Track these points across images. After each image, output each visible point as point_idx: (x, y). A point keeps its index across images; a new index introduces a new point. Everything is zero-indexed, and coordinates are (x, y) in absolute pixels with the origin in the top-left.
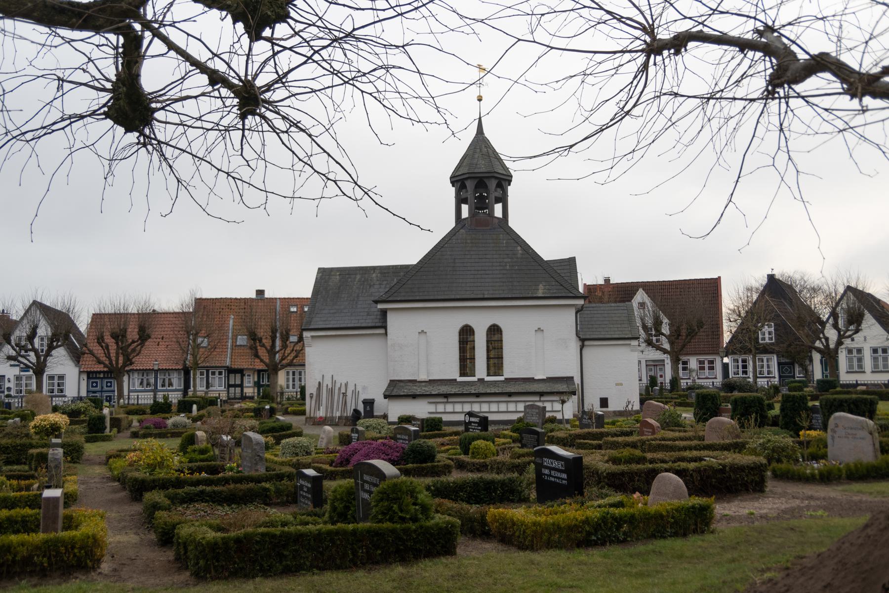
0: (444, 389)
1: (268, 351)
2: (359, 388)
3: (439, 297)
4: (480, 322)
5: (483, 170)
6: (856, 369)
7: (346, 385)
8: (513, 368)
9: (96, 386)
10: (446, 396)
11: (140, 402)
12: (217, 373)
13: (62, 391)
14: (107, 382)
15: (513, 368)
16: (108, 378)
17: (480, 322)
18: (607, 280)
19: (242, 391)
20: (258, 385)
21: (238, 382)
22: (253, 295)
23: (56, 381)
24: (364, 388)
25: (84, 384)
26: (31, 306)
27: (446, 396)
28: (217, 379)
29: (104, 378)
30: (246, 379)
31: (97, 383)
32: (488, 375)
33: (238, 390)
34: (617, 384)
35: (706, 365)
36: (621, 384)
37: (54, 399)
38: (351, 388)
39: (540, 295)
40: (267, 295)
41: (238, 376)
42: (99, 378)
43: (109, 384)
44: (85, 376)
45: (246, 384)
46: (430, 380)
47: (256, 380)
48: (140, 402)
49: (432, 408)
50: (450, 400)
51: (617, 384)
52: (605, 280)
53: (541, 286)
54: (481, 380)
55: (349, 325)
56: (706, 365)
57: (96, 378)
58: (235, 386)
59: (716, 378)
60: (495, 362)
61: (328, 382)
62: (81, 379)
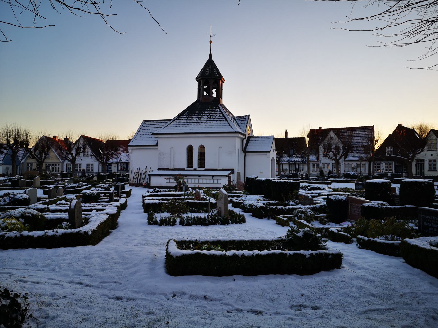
6: (433, 169)
11: (278, 170)
14: (109, 167)
16: (110, 165)
18: (320, 128)
22: (318, 128)
23: (90, 166)
25: (101, 167)
26: (80, 137)
29: (108, 165)
35: (316, 166)
37: (121, 172)
43: (110, 168)
44: (101, 165)
48: (278, 170)
52: (320, 127)
56: (316, 166)
59: (365, 172)
60: (202, 163)
62: (100, 166)
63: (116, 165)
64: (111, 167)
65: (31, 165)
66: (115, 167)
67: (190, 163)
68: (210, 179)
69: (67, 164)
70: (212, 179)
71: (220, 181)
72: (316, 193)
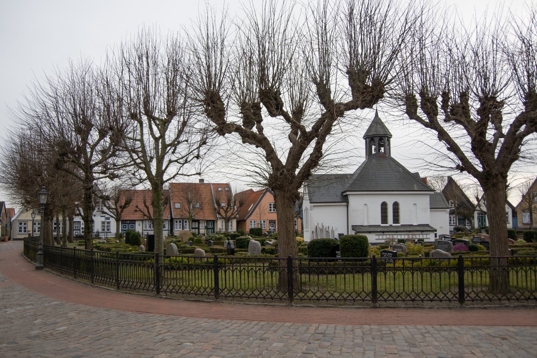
0: (422, 229)
1: (225, 211)
2: (334, 229)
3: (364, 190)
4: (390, 201)
5: (382, 133)
7: (328, 227)
8: (404, 220)
9: (126, 228)
10: (383, 232)
12: (178, 222)
13: (108, 230)
15: (404, 220)
16: (131, 223)
17: (390, 201)
19: (199, 231)
20: (206, 228)
21: (197, 226)
24: (336, 229)
27: (423, 231)
28: (178, 225)
29: (130, 223)
30: (201, 225)
31: (126, 226)
32: (382, 223)
33: (197, 230)
34: (441, 228)
36: (442, 228)
38: (330, 229)
39: (416, 189)
40: (205, 182)
41: (197, 223)
42: (127, 223)
43: (132, 227)
45: (201, 228)
46: (369, 226)
47: (206, 225)
48: (108, 236)
49: (377, 237)
50: (385, 234)
51: (441, 228)
53: (415, 186)
54: (391, 225)
55: (330, 201)
57: (125, 223)
58: (195, 228)
60: (396, 219)
61: (320, 226)
63: (141, 223)
64: (133, 226)
65: (25, 224)
66: (139, 225)
67: (384, 219)
68: (419, 234)
69: (80, 222)
70: (422, 234)
71: (428, 236)
72: (146, 325)
